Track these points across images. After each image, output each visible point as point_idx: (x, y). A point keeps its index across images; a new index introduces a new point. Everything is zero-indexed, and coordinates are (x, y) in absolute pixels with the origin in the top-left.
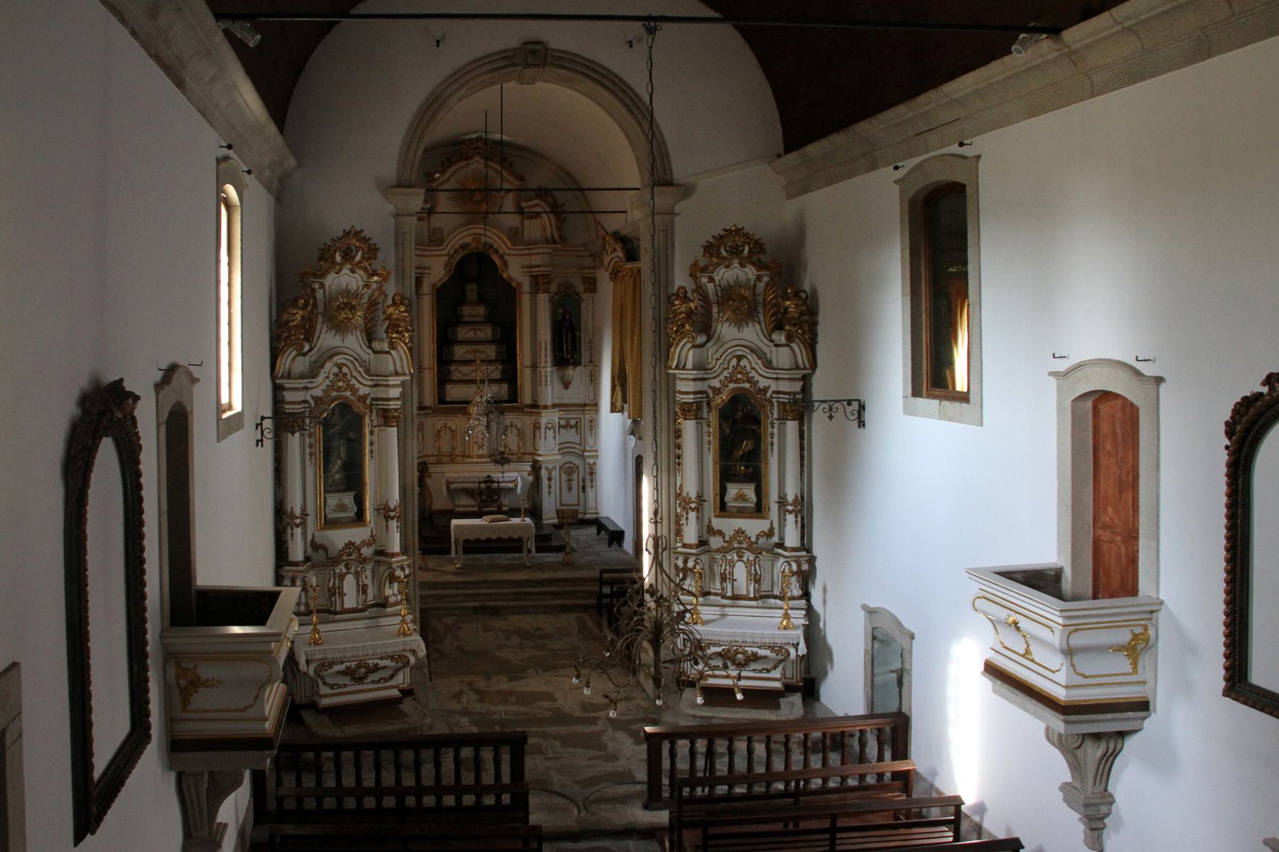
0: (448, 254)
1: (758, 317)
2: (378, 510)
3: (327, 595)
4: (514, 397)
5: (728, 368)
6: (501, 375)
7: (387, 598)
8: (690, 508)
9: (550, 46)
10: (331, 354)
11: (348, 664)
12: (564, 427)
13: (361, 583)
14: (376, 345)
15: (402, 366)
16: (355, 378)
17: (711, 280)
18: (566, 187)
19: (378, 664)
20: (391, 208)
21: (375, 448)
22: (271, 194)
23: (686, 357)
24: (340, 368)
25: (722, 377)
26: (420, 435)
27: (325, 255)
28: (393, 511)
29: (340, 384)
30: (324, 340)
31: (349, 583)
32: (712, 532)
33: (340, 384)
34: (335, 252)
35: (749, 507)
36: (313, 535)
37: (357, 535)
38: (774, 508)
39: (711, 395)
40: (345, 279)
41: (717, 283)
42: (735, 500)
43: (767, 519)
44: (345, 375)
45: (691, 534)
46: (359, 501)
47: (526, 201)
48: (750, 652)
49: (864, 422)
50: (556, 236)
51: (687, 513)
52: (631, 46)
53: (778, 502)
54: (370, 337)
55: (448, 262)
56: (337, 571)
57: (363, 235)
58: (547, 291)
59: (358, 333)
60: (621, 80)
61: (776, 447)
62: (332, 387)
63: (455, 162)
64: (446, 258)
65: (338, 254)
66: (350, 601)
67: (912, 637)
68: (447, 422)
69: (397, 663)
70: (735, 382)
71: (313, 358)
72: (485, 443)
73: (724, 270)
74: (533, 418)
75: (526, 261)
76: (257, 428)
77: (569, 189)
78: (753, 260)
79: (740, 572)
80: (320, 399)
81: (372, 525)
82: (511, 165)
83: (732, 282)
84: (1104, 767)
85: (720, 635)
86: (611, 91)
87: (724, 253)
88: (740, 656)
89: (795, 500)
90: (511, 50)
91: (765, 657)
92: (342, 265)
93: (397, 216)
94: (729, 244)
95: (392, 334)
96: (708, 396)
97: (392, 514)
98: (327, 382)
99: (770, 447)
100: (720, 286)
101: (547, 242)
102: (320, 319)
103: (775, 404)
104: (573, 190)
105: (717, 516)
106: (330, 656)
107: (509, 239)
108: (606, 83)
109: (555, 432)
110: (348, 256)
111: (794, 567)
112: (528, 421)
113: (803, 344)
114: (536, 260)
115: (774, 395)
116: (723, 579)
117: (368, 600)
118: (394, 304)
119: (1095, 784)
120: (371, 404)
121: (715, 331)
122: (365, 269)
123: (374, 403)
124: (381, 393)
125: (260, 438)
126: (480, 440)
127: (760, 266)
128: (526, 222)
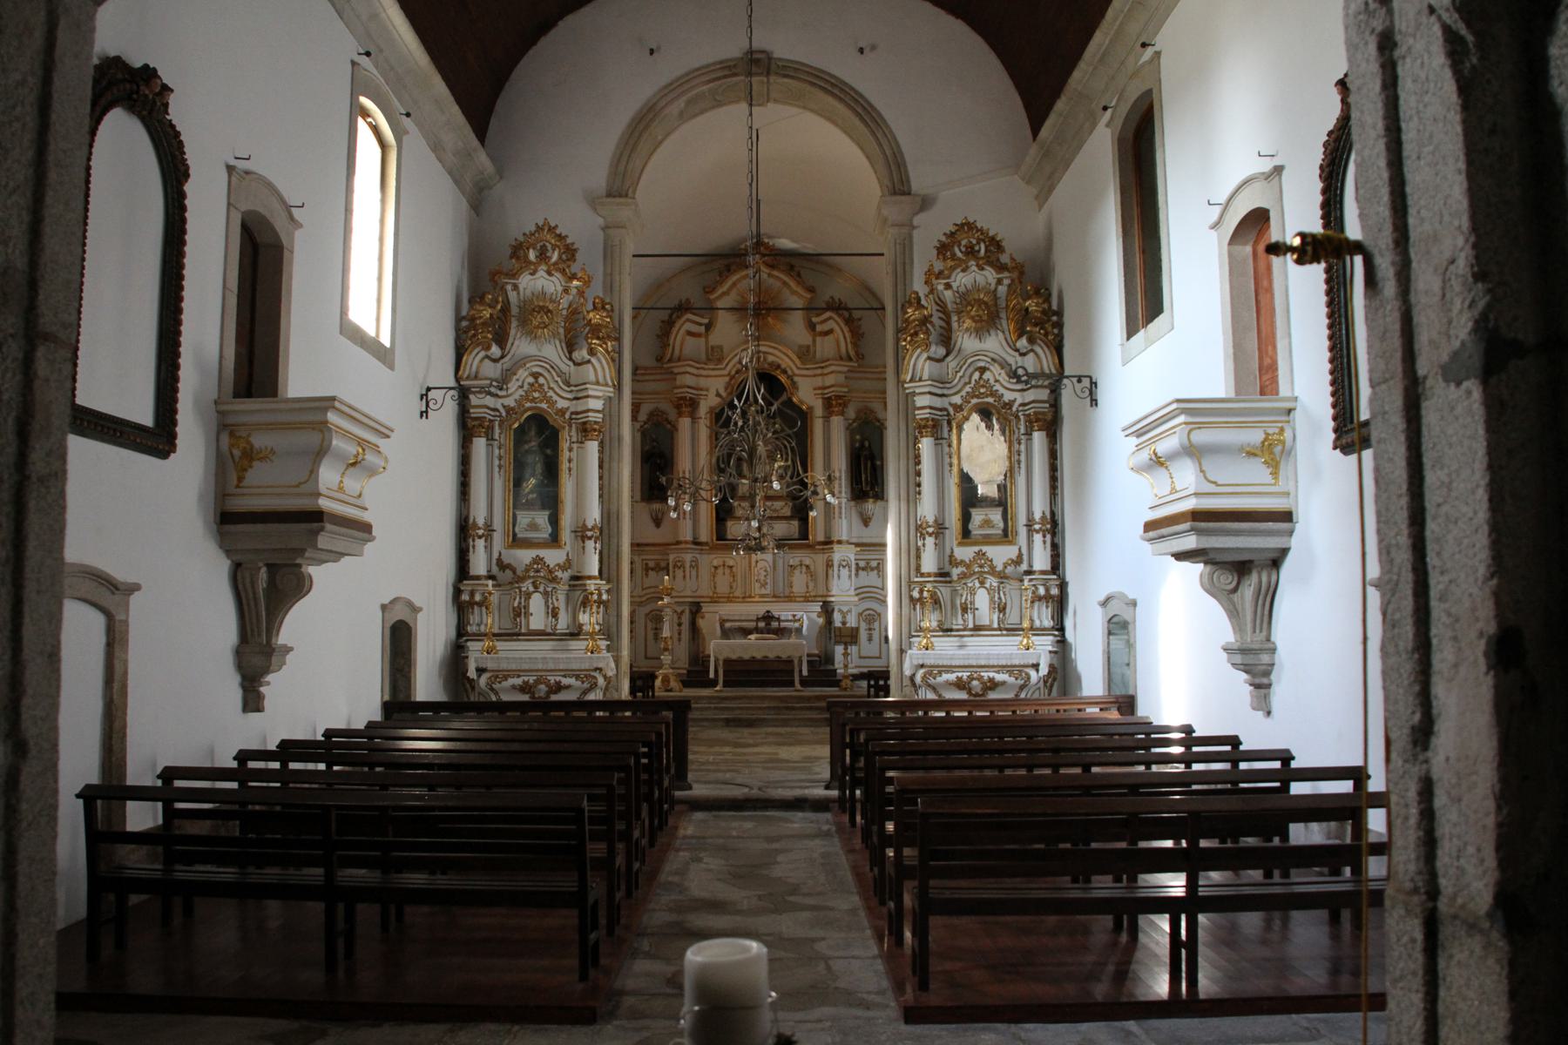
0: (729, 374)
1: (1001, 325)
2: (575, 532)
3: (512, 615)
4: (804, 534)
5: (970, 383)
6: (792, 512)
7: (581, 626)
8: (927, 533)
9: (775, 56)
10: (521, 362)
11: (526, 679)
12: (863, 569)
13: (551, 606)
14: (576, 355)
15: (605, 376)
16: (552, 389)
17: (948, 286)
18: (867, 306)
19: (560, 682)
20: (601, 221)
21: (573, 465)
22: (463, 194)
23: (923, 369)
24: (536, 378)
25: (963, 393)
26: (694, 573)
27: (518, 251)
28: (590, 530)
29: (536, 395)
30: (518, 346)
31: (536, 603)
32: (953, 562)
33: (536, 395)
34: (528, 249)
35: (996, 535)
36: (500, 554)
37: (553, 557)
38: (1023, 531)
39: (952, 412)
40: (538, 283)
41: (955, 289)
42: (981, 527)
43: (1015, 544)
44: (541, 386)
45: (929, 563)
46: (554, 521)
47: (818, 315)
48: (986, 678)
49: (1096, 400)
50: (852, 353)
51: (924, 539)
52: (862, 53)
53: (1026, 525)
54: (570, 347)
55: (728, 384)
56: (524, 589)
57: (558, 232)
58: (842, 413)
59: (557, 342)
60: (852, 89)
61: (1023, 465)
62: (526, 397)
63: (735, 271)
64: (727, 379)
65: (531, 251)
66: (537, 620)
67: (1134, 604)
68: (727, 560)
69: (583, 682)
70: (978, 397)
71: (505, 367)
72: (768, 581)
73: (961, 274)
74: (826, 556)
75: (819, 381)
76: (422, 399)
77: (872, 309)
78: (991, 260)
79: (982, 600)
80: (513, 409)
81: (568, 548)
82: (799, 275)
83: (969, 287)
84: (1264, 605)
85: (951, 659)
86: (841, 100)
87: (959, 254)
88: (975, 683)
89: (1043, 517)
90: (731, 60)
91: (1004, 683)
92: (536, 265)
93: (605, 228)
94: (964, 243)
95: (592, 339)
96: (948, 415)
97: (589, 534)
98: (521, 392)
99: (1017, 465)
100: (958, 292)
101: (841, 359)
102: (514, 324)
103: (1022, 417)
104: (876, 309)
105: (960, 544)
106: (504, 666)
107: (799, 358)
108: (836, 91)
109: (850, 571)
110: (543, 256)
111: (1042, 591)
112: (819, 559)
113: (1048, 347)
114: (830, 380)
115: (1021, 408)
116: (965, 610)
117: (558, 627)
118: (595, 308)
119: (1254, 632)
120: (571, 419)
121: (956, 342)
122: (563, 272)
123: (574, 416)
124: (580, 406)
125: (424, 409)
126: (762, 578)
127: (1001, 268)
128: (819, 339)
